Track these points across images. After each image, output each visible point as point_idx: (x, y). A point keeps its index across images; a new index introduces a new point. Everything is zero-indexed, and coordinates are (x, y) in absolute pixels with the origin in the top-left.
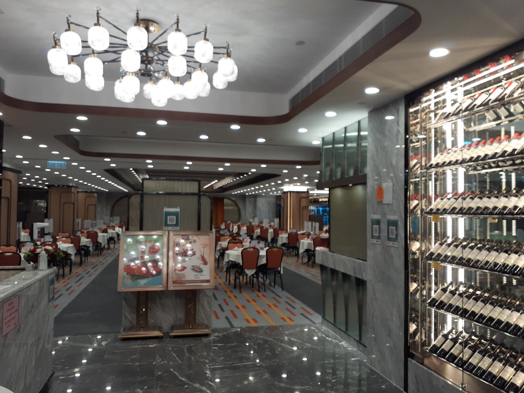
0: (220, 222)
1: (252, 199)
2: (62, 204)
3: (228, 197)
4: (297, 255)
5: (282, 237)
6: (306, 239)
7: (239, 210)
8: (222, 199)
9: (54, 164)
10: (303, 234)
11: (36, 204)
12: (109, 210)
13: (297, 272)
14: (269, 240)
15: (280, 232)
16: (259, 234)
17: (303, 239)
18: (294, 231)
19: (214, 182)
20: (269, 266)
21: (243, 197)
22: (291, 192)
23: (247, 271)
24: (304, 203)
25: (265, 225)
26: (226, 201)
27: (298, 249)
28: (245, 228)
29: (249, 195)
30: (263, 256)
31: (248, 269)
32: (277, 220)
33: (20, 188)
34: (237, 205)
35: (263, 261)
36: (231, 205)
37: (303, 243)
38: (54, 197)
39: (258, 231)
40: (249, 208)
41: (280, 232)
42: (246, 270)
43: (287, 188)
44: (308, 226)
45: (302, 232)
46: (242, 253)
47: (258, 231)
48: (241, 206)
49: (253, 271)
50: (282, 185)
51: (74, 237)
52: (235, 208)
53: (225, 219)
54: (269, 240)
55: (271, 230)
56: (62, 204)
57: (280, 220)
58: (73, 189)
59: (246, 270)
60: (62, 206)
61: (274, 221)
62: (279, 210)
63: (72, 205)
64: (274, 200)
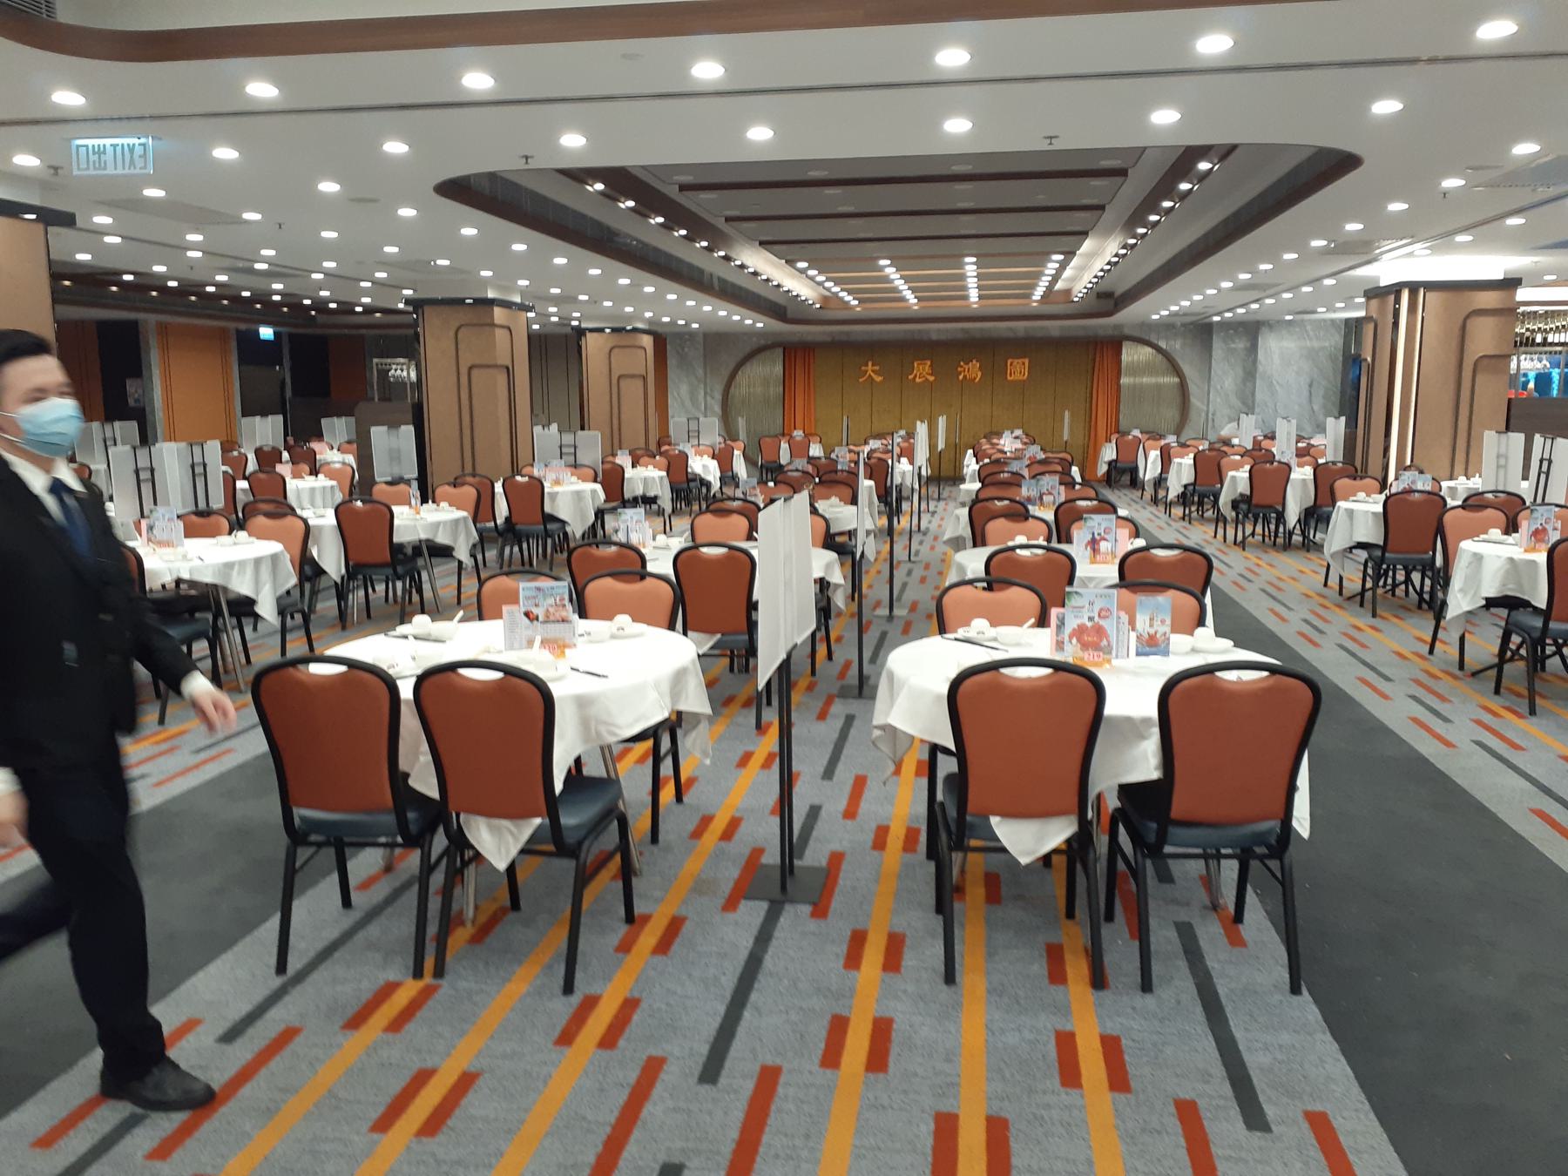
0: (1102, 432)
1: (1240, 345)
2: (464, 370)
3: (1136, 334)
4: (1435, 607)
5: (1350, 513)
6: (1495, 533)
7: (1183, 387)
8: (1113, 344)
9: (100, 152)
10: (1474, 502)
11: (384, 374)
12: (718, 396)
13: (1427, 747)
14: (1293, 514)
15: (1342, 484)
16: (1243, 487)
17: (1472, 534)
18: (1423, 484)
19: (1051, 267)
20: (1178, 808)
21: (1201, 331)
22: (1414, 287)
23: (1007, 831)
24: (1484, 337)
25: (1283, 449)
26: (1132, 354)
27: (1443, 578)
28: (1188, 460)
29: (1225, 325)
30: (1131, 728)
31: (1007, 814)
32: (1337, 426)
33: (532, 338)
34: (1176, 370)
35: (1145, 764)
36: (1148, 369)
37: (1478, 558)
38: (436, 338)
39: (1238, 479)
40: (1225, 373)
41: (1342, 484)
42: (994, 820)
43: (1396, 264)
44: (1500, 460)
45: (1463, 485)
46: (955, 685)
47: (1238, 479)
48: (1187, 369)
49: (1056, 833)
50: (1363, 249)
51: (369, 506)
52: (1177, 380)
53: (1124, 423)
54: (1293, 514)
55: (1302, 474)
56: (464, 370)
57: (1352, 424)
58: (499, 314)
59: (994, 820)
60: (464, 379)
61: (1321, 429)
62: (1355, 383)
63: (502, 379)
64: (1335, 340)
